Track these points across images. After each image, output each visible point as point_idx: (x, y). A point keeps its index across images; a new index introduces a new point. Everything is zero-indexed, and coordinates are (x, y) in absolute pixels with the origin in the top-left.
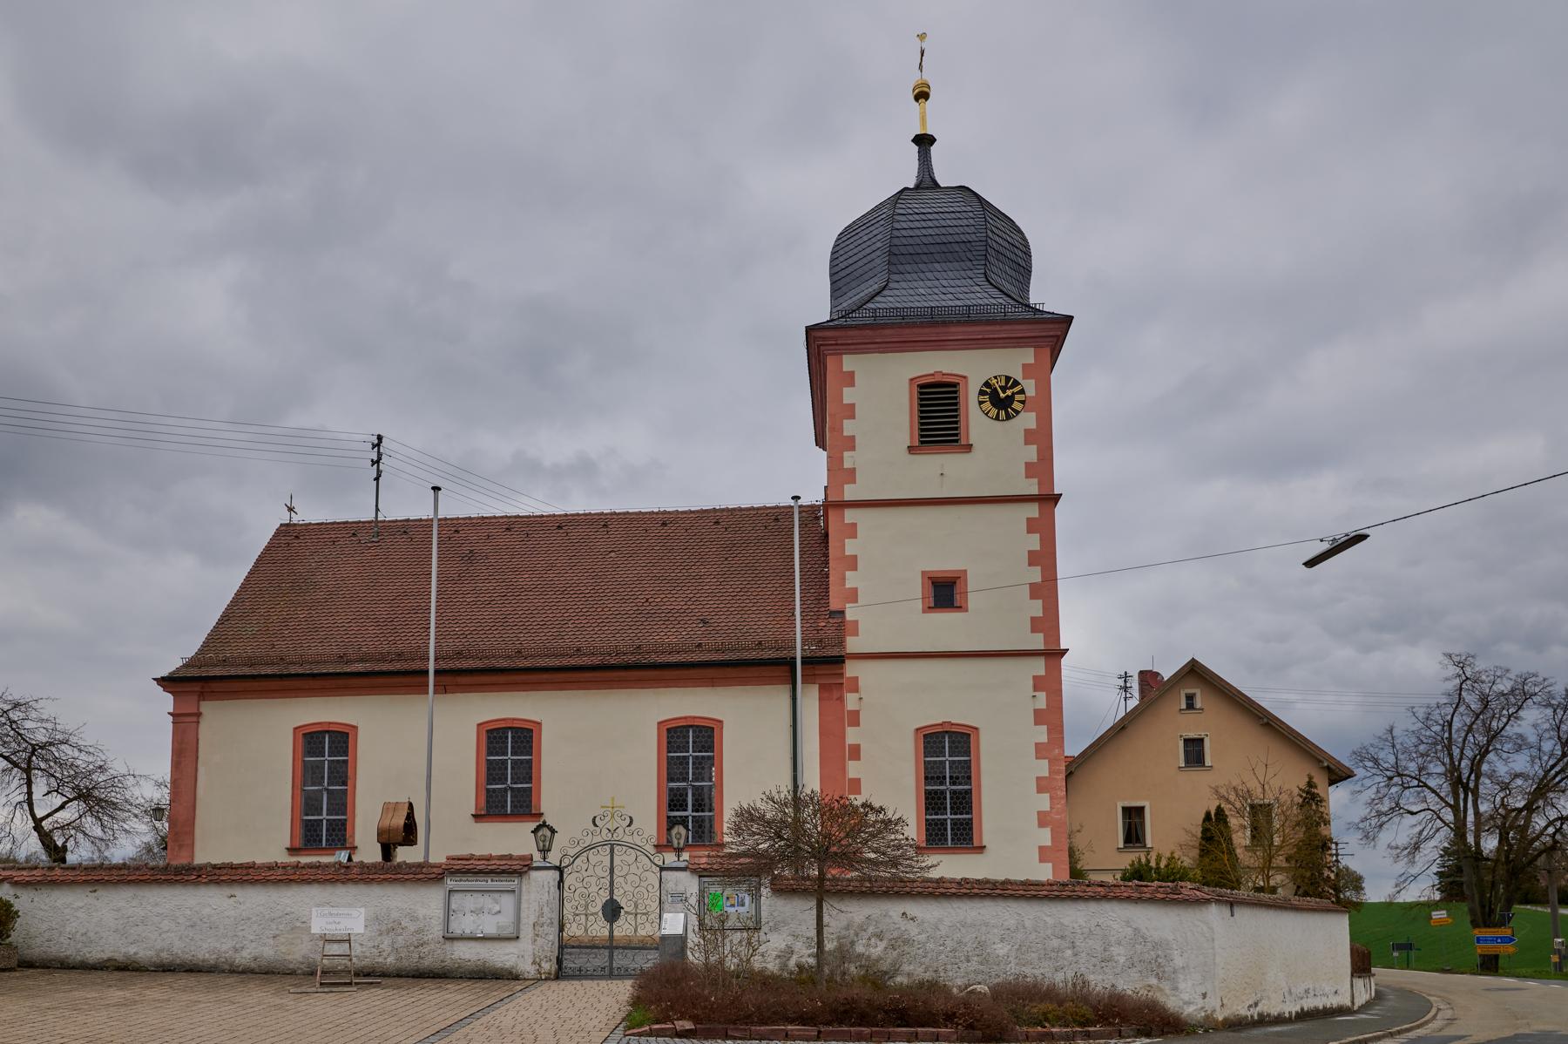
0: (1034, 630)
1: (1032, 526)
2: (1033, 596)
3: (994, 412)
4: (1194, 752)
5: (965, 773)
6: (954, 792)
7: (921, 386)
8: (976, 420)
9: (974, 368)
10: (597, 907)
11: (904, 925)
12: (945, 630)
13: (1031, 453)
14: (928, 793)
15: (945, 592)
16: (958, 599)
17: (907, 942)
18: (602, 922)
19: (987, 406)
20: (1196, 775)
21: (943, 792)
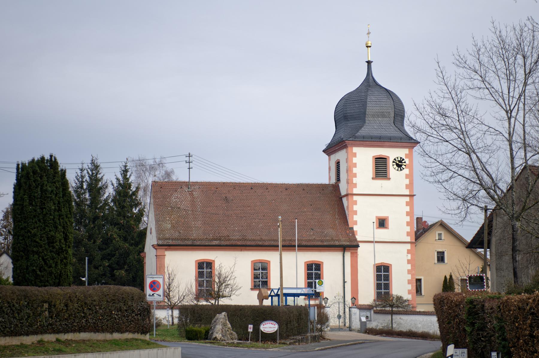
0: (407, 236)
1: (407, 204)
2: (407, 225)
3: (397, 168)
4: (441, 258)
5: (387, 278)
6: (384, 284)
7: (376, 158)
8: (392, 169)
9: (392, 154)
10: (336, 316)
11: (400, 320)
12: (382, 234)
13: (407, 181)
14: (377, 284)
15: (382, 223)
16: (386, 225)
17: (401, 324)
18: (337, 319)
19: (395, 166)
20: (441, 265)
21: (381, 283)
